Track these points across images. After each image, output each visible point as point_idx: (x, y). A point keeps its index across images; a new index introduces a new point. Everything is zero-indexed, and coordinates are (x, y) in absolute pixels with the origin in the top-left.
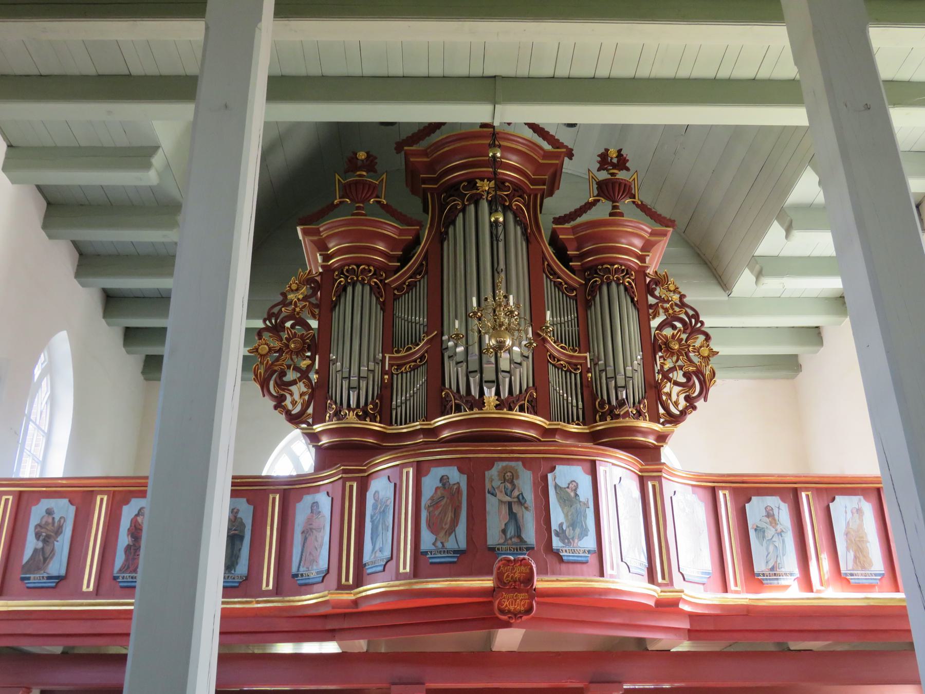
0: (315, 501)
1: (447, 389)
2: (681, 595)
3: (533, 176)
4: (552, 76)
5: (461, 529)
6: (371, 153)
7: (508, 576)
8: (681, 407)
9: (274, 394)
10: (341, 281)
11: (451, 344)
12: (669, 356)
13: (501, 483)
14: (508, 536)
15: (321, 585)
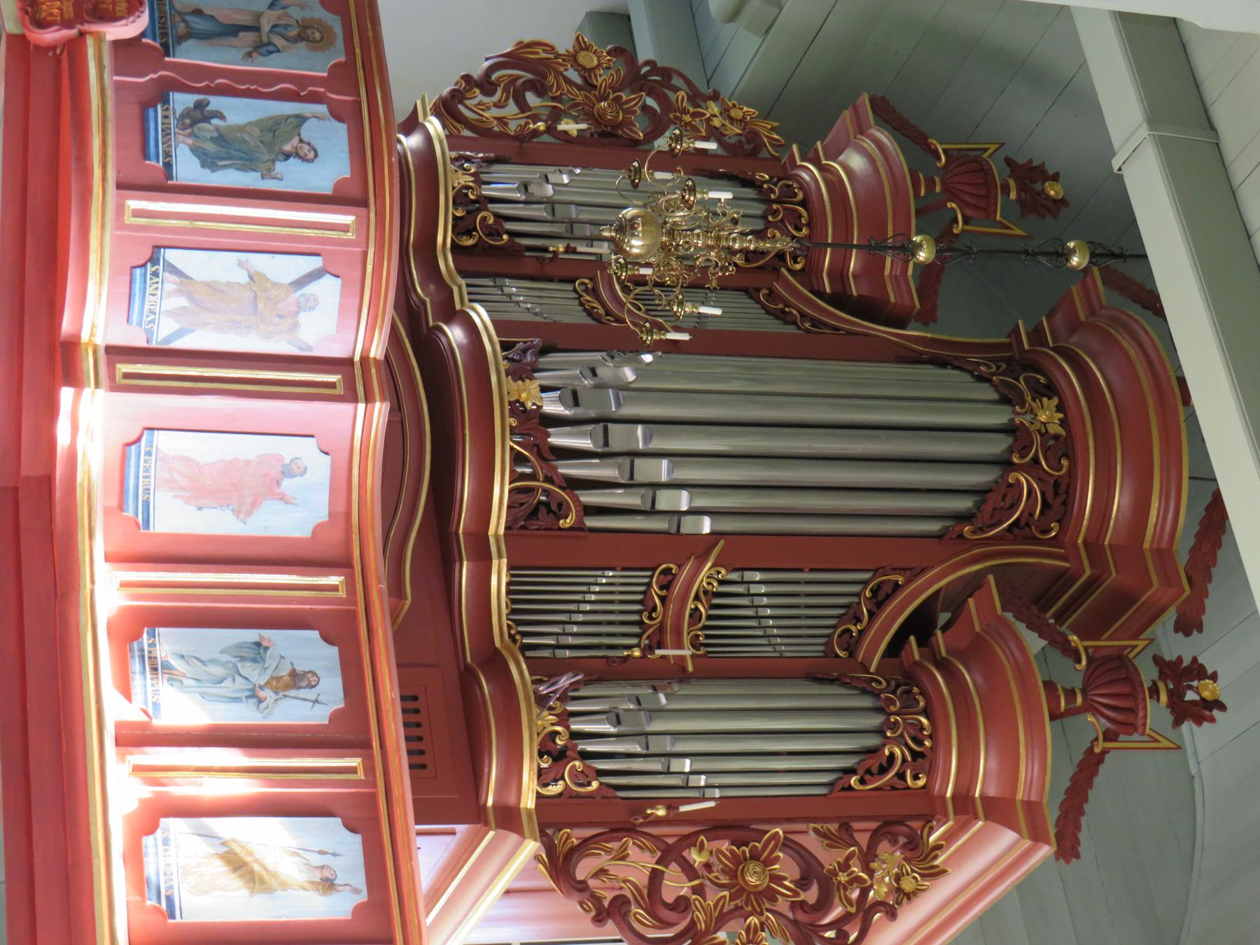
9: (494, 77)
13: (297, 21)
14: (188, 18)
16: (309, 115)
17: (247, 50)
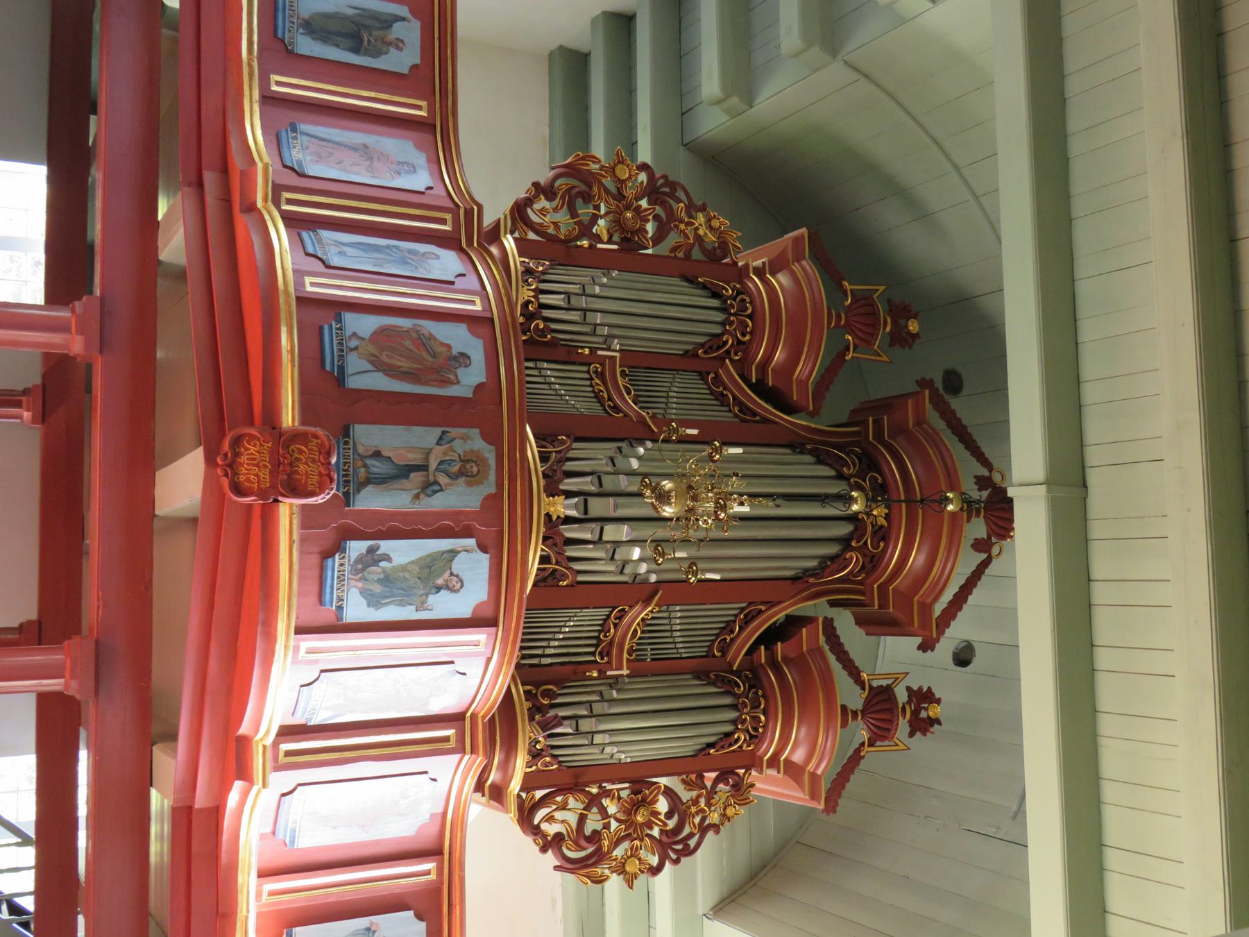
0: (418, 170)
1: (571, 444)
2: (258, 784)
3: (893, 589)
4: (1091, 578)
5: (381, 382)
6: (917, 341)
7: (301, 452)
8: (544, 826)
9: (558, 183)
10: (727, 290)
11: (641, 450)
12: (625, 807)
13: (459, 455)
14: (368, 462)
15: (280, 167)
16: (461, 549)
17: (416, 491)
